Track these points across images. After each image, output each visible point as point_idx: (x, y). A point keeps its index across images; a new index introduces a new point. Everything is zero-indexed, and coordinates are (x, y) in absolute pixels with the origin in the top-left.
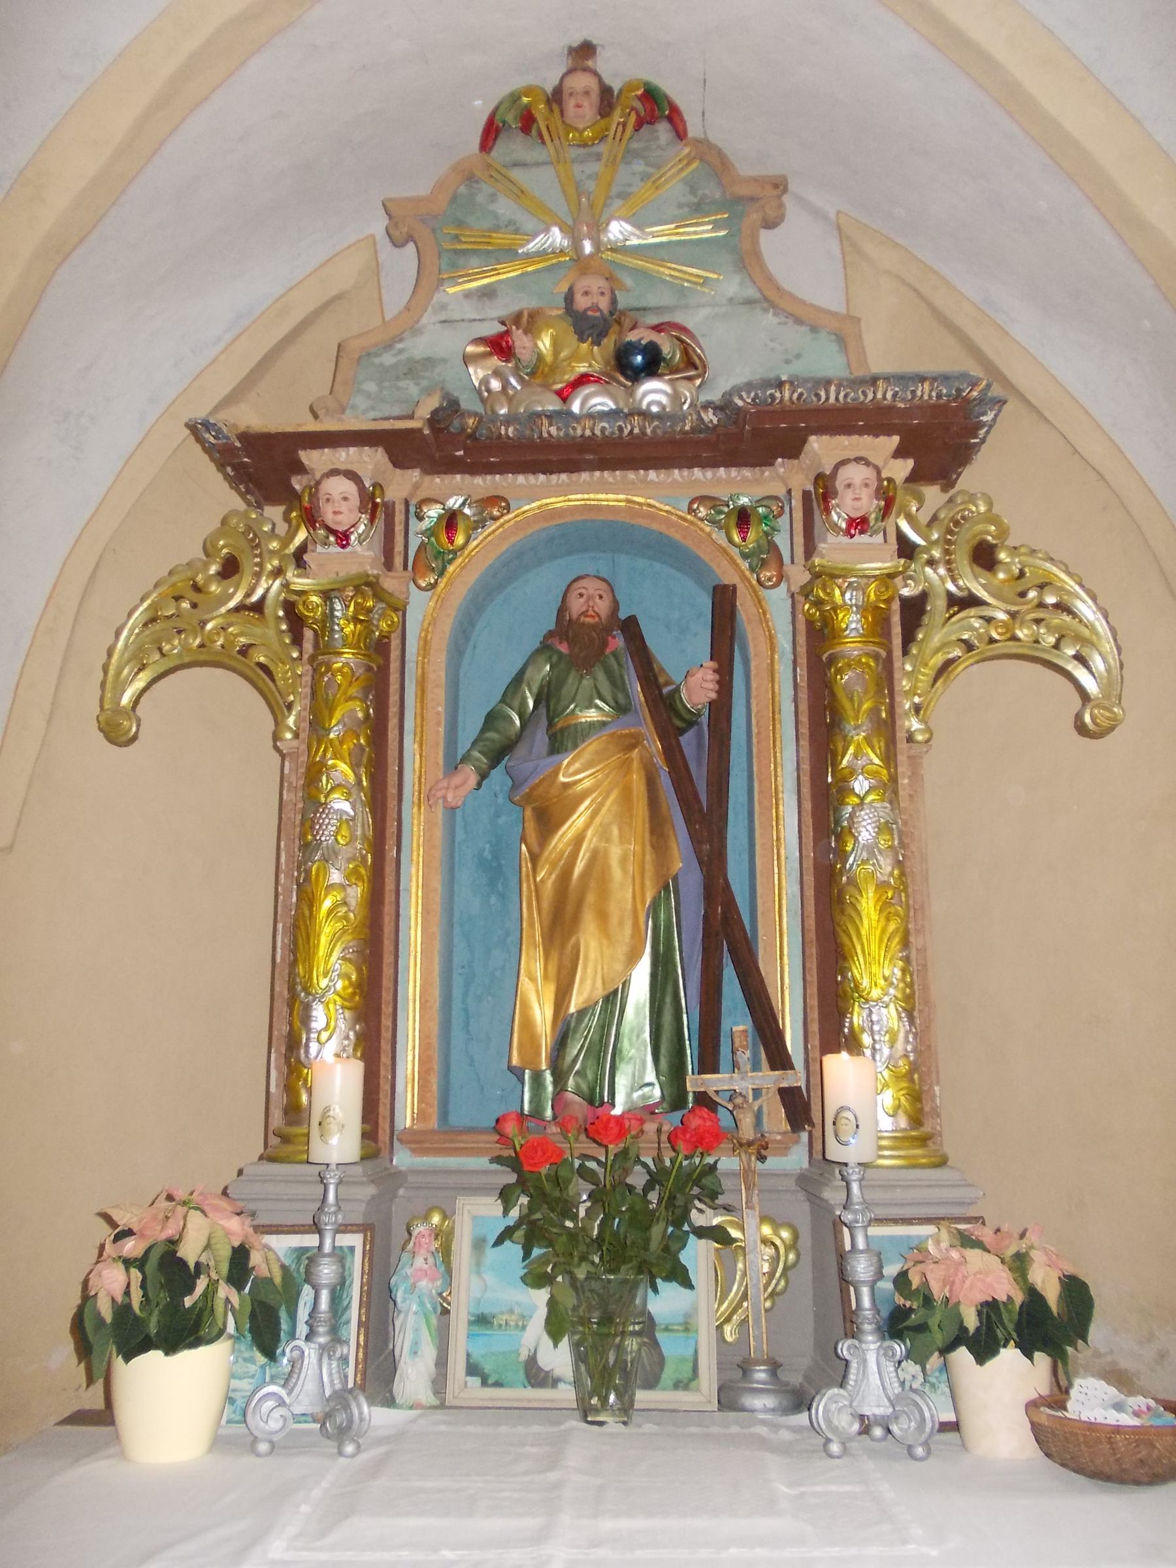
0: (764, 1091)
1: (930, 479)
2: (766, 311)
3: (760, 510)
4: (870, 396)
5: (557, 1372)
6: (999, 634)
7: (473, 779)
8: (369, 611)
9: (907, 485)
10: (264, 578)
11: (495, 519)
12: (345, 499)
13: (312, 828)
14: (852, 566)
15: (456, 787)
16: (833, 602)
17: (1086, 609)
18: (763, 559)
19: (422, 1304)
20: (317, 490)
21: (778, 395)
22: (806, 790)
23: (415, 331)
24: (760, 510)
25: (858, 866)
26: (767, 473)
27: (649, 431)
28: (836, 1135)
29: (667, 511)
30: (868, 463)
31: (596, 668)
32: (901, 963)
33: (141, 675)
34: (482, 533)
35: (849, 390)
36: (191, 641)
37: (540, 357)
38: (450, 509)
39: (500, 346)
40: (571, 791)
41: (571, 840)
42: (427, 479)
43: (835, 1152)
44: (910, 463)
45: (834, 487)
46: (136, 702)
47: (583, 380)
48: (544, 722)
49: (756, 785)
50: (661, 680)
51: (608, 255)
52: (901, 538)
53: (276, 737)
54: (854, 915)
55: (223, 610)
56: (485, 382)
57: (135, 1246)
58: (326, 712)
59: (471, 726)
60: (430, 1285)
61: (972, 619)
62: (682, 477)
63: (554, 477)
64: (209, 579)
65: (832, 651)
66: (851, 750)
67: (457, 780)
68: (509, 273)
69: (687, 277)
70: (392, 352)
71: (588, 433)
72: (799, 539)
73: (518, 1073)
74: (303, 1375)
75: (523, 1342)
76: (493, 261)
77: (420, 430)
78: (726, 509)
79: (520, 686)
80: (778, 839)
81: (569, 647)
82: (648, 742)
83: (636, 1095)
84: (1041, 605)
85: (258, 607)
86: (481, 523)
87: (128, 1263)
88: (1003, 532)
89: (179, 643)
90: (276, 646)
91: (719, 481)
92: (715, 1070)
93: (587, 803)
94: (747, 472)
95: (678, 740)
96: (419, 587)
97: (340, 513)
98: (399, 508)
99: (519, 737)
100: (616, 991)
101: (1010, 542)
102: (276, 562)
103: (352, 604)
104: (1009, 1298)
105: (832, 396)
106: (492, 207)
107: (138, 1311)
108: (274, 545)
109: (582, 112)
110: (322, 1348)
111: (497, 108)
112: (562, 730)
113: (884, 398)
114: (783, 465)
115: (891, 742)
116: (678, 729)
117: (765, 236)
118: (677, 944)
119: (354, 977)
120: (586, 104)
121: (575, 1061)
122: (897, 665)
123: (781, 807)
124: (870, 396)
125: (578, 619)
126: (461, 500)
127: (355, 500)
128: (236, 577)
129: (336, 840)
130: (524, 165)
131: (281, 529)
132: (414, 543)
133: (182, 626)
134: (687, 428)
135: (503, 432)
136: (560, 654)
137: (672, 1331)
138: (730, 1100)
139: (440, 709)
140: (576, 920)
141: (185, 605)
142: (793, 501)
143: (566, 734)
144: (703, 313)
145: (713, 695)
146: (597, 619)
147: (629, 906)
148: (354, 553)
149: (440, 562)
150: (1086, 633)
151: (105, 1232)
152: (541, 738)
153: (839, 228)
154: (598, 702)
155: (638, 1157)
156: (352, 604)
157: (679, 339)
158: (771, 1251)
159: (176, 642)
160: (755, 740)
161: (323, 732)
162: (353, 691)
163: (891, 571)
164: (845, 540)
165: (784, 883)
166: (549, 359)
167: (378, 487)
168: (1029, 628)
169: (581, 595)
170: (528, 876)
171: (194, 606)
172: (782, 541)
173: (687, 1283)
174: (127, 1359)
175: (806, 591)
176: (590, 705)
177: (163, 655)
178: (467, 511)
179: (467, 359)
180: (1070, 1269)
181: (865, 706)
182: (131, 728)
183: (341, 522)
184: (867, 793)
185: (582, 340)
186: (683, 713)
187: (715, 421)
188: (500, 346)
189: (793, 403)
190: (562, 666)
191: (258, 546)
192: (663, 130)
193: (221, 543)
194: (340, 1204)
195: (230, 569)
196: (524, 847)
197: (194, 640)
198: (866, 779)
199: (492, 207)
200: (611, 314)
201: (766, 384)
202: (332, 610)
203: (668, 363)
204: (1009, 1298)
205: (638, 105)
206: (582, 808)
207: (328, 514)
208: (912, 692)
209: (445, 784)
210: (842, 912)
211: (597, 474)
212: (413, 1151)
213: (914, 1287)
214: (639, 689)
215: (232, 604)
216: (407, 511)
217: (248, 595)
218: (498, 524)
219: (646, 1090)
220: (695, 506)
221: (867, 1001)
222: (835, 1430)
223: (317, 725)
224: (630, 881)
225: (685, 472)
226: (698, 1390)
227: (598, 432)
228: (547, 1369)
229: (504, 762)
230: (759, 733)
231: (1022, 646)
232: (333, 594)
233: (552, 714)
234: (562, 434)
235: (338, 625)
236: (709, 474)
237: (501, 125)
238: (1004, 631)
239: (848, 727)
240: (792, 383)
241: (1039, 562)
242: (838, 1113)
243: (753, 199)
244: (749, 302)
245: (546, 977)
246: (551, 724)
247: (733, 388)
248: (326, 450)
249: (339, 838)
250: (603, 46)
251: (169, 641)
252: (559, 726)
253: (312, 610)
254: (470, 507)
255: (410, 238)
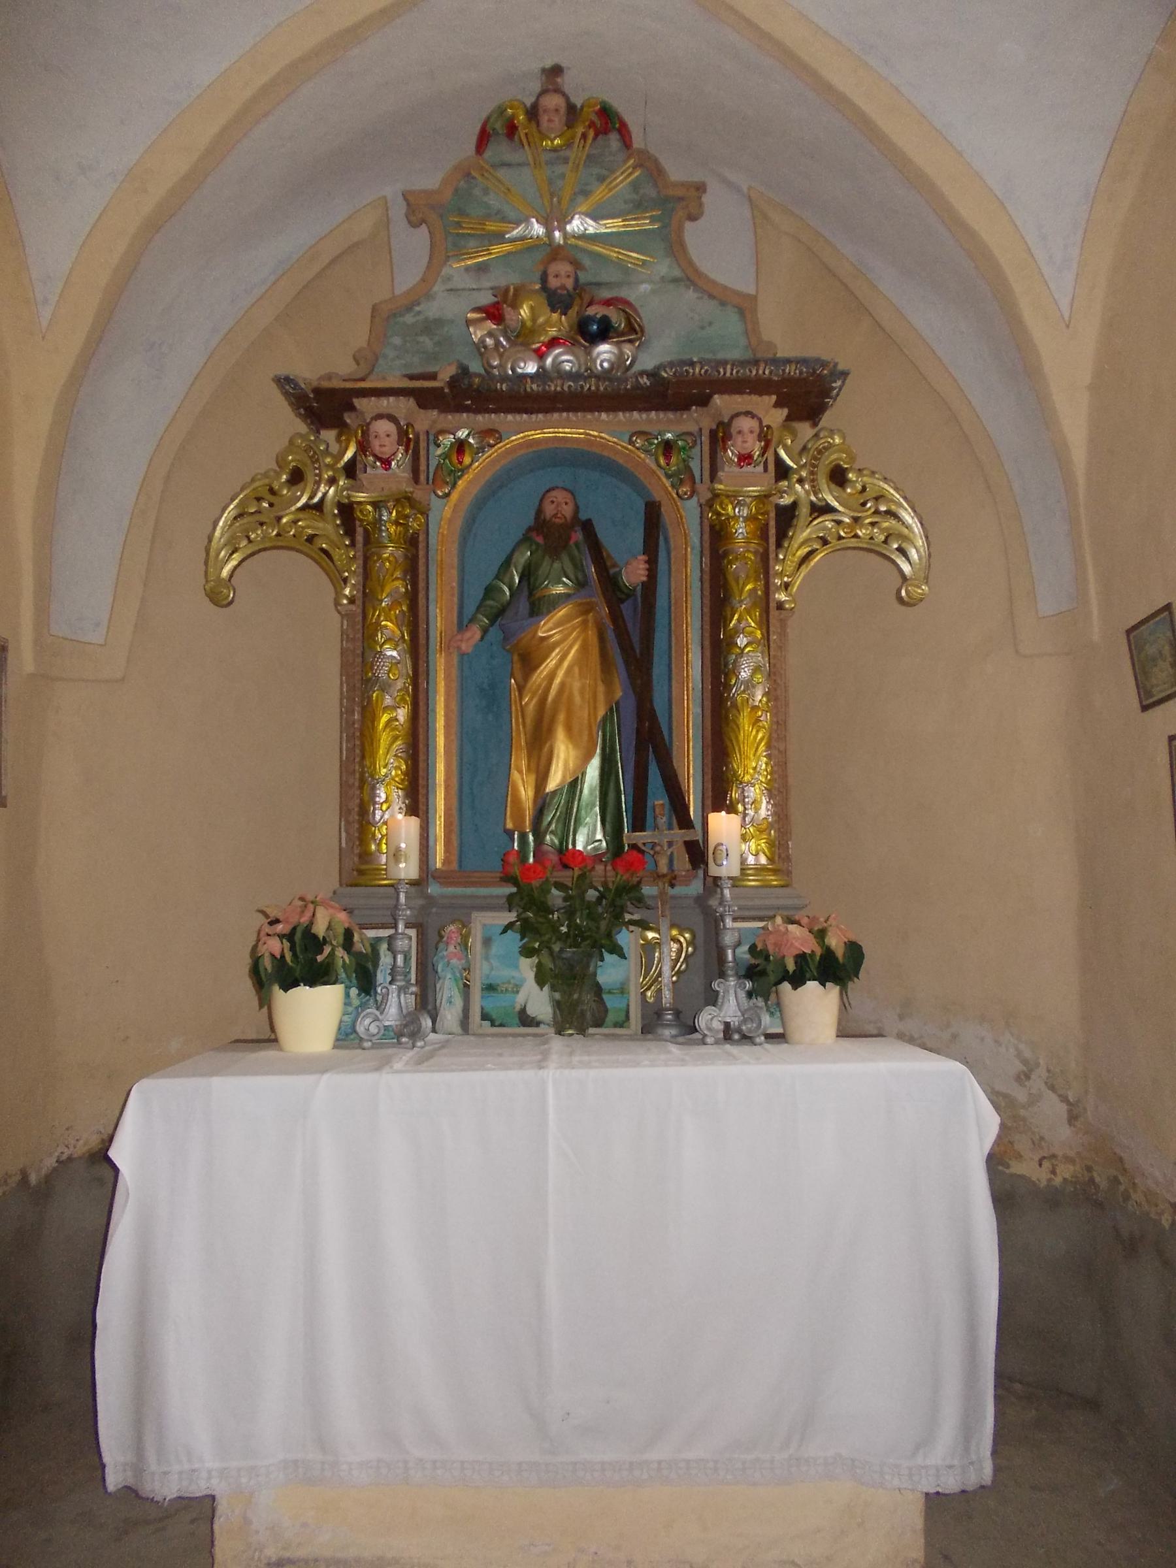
0: (674, 844)
1: (801, 419)
2: (688, 288)
3: (680, 443)
4: (754, 372)
5: (540, 1018)
6: (845, 533)
7: (478, 635)
8: (407, 517)
9: (785, 423)
10: (323, 485)
11: (492, 446)
12: (388, 436)
13: (372, 669)
14: (740, 489)
15: (469, 639)
16: (728, 514)
17: (908, 516)
18: (681, 479)
19: (454, 973)
20: (368, 429)
21: (691, 371)
22: (707, 643)
23: (429, 296)
24: (680, 443)
25: (738, 695)
26: (685, 416)
27: (602, 388)
28: (714, 860)
29: (614, 443)
30: (753, 416)
31: (563, 555)
32: (765, 759)
33: (234, 556)
34: (483, 455)
35: (739, 368)
36: (271, 531)
37: (523, 322)
38: (459, 438)
39: (493, 313)
40: (546, 643)
41: (547, 675)
42: (443, 415)
43: (714, 870)
44: (785, 411)
45: (730, 432)
46: (231, 576)
47: (553, 343)
48: (526, 593)
49: (673, 639)
50: (608, 564)
51: (572, 241)
52: (779, 462)
53: (337, 603)
54: (735, 727)
55: (293, 509)
56: (482, 341)
57: (283, 927)
58: (379, 589)
59: (475, 594)
60: (458, 962)
61: (827, 522)
62: (624, 417)
63: (534, 416)
64: (282, 485)
65: (724, 548)
66: (736, 617)
67: (468, 635)
68: (497, 249)
69: (630, 260)
70: (412, 314)
71: (559, 389)
72: (707, 465)
73: (510, 833)
74: (388, 1004)
75: (517, 1000)
76: (486, 242)
77: (442, 388)
78: (656, 441)
79: (510, 567)
80: (688, 676)
81: (545, 539)
82: (599, 608)
83: (589, 847)
84: (877, 512)
85: (319, 507)
86: (481, 449)
87: (281, 936)
88: (852, 458)
89: (262, 533)
90: (334, 537)
91: (650, 421)
92: (643, 829)
93: (557, 650)
94: (671, 415)
95: (619, 607)
96: (439, 497)
97: (384, 446)
98: (422, 437)
99: (509, 603)
100: (578, 778)
101: (857, 466)
102: (330, 473)
103: (394, 512)
104: (813, 951)
105: (729, 372)
106: (485, 199)
107: (290, 964)
108: (328, 460)
109: (553, 121)
110: (400, 989)
111: (488, 118)
112: (539, 599)
113: (764, 373)
114: (696, 411)
115: (766, 611)
116: (620, 599)
117: (688, 225)
118: (618, 747)
119: (404, 767)
120: (556, 119)
121: (550, 823)
122: (772, 556)
123: (690, 655)
124: (754, 372)
125: (551, 519)
126: (466, 433)
127: (395, 436)
128: (302, 485)
129: (389, 677)
130: (509, 165)
131: (335, 448)
132: (433, 463)
133: (264, 520)
134: (629, 387)
135: (498, 387)
136: (538, 545)
137: (614, 993)
138: (652, 849)
139: (454, 584)
140: (550, 731)
141: (265, 505)
142: (703, 438)
143: (542, 603)
144: (645, 287)
145: (644, 579)
146: (563, 520)
147: (586, 722)
148: (394, 474)
149: (452, 478)
150: (906, 531)
151: (263, 920)
152: (523, 606)
153: (750, 200)
154: (564, 579)
155: (591, 883)
156: (394, 512)
157: (623, 311)
158: (675, 946)
159: (259, 532)
160: (673, 608)
161: (378, 603)
162: (398, 574)
163: (766, 493)
164: (736, 469)
165: (691, 706)
166: (529, 324)
167: (410, 426)
168: (867, 529)
169: (553, 502)
170: (516, 702)
171: (271, 505)
172: (695, 465)
173: (622, 956)
174: (286, 990)
175: (710, 504)
176: (560, 582)
177: (250, 541)
178: (471, 441)
179: (469, 322)
180: (853, 938)
181: (749, 587)
182: (229, 596)
183: (386, 452)
184: (746, 646)
185: (553, 310)
186: (626, 591)
187: (648, 384)
188: (493, 313)
189: (701, 375)
190: (540, 552)
191: (317, 461)
192: (614, 140)
193: (290, 458)
194: (393, 921)
195: (297, 477)
196: (513, 681)
197: (273, 531)
198: (746, 637)
199: (485, 199)
200: (575, 289)
201: (683, 363)
202: (381, 515)
203: (616, 329)
204: (813, 951)
205: (594, 118)
206: (554, 654)
207: (376, 445)
208: (781, 574)
209: (459, 637)
210: (728, 724)
211: (565, 414)
212: (441, 884)
213: (758, 949)
214: (593, 570)
215: (299, 504)
216: (428, 440)
217: (311, 498)
218: (493, 450)
219: (596, 844)
220: (634, 438)
221: (741, 783)
222: (710, 1029)
223: (368, 595)
224: (587, 704)
225: (627, 415)
226: (629, 1027)
227: (566, 388)
228: (534, 1016)
229: (498, 623)
230: (676, 603)
231: (861, 542)
232: (381, 504)
233: (531, 587)
234: (540, 389)
235: (385, 526)
236: (644, 416)
237: (491, 132)
238: (849, 531)
239: (734, 601)
240: (701, 363)
241: (876, 481)
242: (715, 848)
243: (681, 199)
244: (676, 280)
245: (529, 769)
246: (531, 594)
247: (661, 364)
248: (373, 398)
249: (391, 675)
250: (569, 68)
251: (254, 531)
252: (537, 596)
253: (366, 516)
254: (473, 438)
255: (423, 221)
